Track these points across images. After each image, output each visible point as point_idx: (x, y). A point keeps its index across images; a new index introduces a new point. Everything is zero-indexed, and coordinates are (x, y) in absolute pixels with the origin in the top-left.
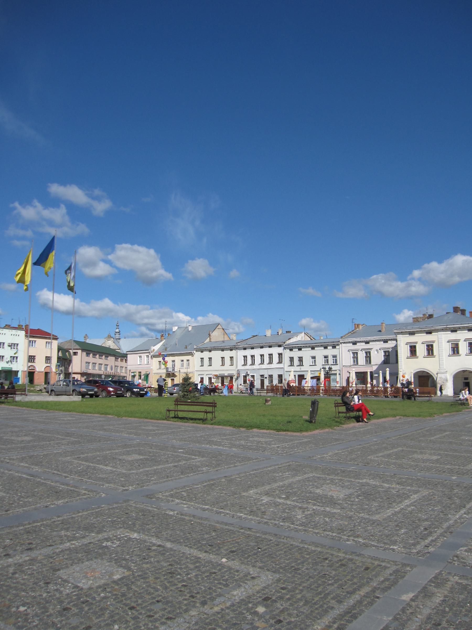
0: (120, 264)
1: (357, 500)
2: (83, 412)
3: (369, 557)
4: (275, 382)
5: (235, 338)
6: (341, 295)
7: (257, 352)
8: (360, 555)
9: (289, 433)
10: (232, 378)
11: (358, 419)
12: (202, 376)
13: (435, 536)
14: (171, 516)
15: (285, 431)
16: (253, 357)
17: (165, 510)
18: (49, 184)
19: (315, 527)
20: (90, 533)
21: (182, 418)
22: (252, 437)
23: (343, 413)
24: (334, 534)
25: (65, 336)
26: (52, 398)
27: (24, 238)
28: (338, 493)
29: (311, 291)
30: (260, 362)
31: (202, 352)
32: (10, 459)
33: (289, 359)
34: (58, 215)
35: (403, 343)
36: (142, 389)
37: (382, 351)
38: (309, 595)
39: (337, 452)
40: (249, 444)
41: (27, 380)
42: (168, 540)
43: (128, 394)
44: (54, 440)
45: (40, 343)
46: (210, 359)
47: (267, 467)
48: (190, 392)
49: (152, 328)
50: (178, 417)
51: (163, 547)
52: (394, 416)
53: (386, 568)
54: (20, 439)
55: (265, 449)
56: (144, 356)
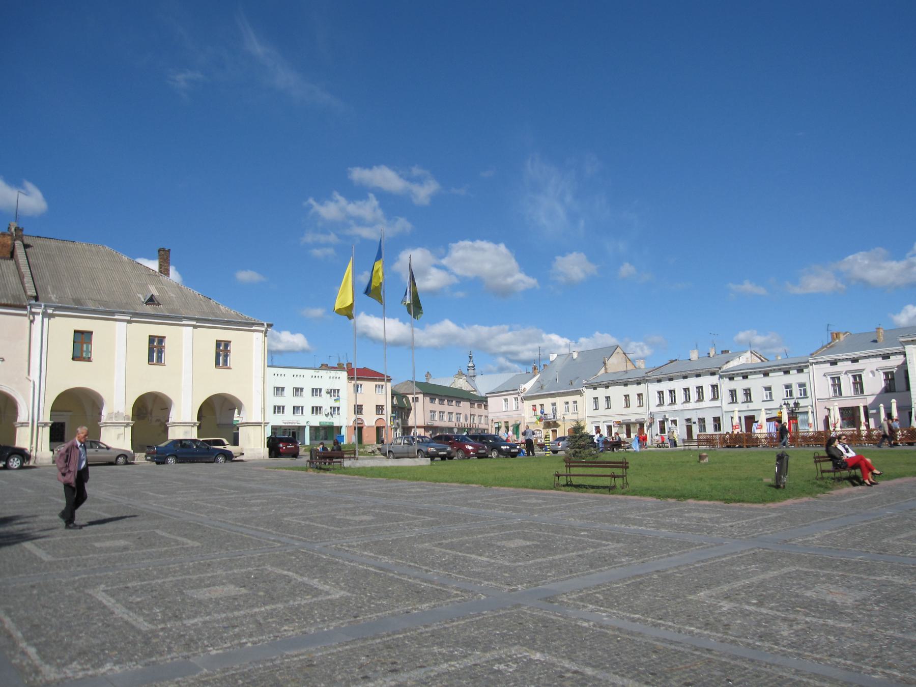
0: (458, 271)
1: (877, 608)
2: (436, 481)
4: (710, 429)
5: (643, 366)
6: (797, 290)
7: (678, 385)
9: (745, 505)
10: (642, 425)
11: (855, 481)
12: (597, 425)
15: (739, 501)
16: (672, 392)
17: (576, 620)
18: (349, 169)
19: (815, 649)
20: (473, 650)
21: (578, 486)
22: (688, 512)
23: (829, 471)
24: (849, 662)
25: (402, 374)
26: (391, 463)
27: (327, 245)
29: (748, 286)
30: (683, 399)
31: (595, 388)
32: (349, 546)
33: (729, 393)
34: (368, 209)
36: (513, 446)
37: (881, 373)
39: (828, 532)
40: (685, 522)
43: (494, 454)
44: (402, 520)
45: (368, 386)
46: (608, 398)
47: (719, 557)
48: (584, 447)
49: (516, 358)
50: (571, 485)
51: (581, 673)
54: (357, 518)
56: (511, 398)
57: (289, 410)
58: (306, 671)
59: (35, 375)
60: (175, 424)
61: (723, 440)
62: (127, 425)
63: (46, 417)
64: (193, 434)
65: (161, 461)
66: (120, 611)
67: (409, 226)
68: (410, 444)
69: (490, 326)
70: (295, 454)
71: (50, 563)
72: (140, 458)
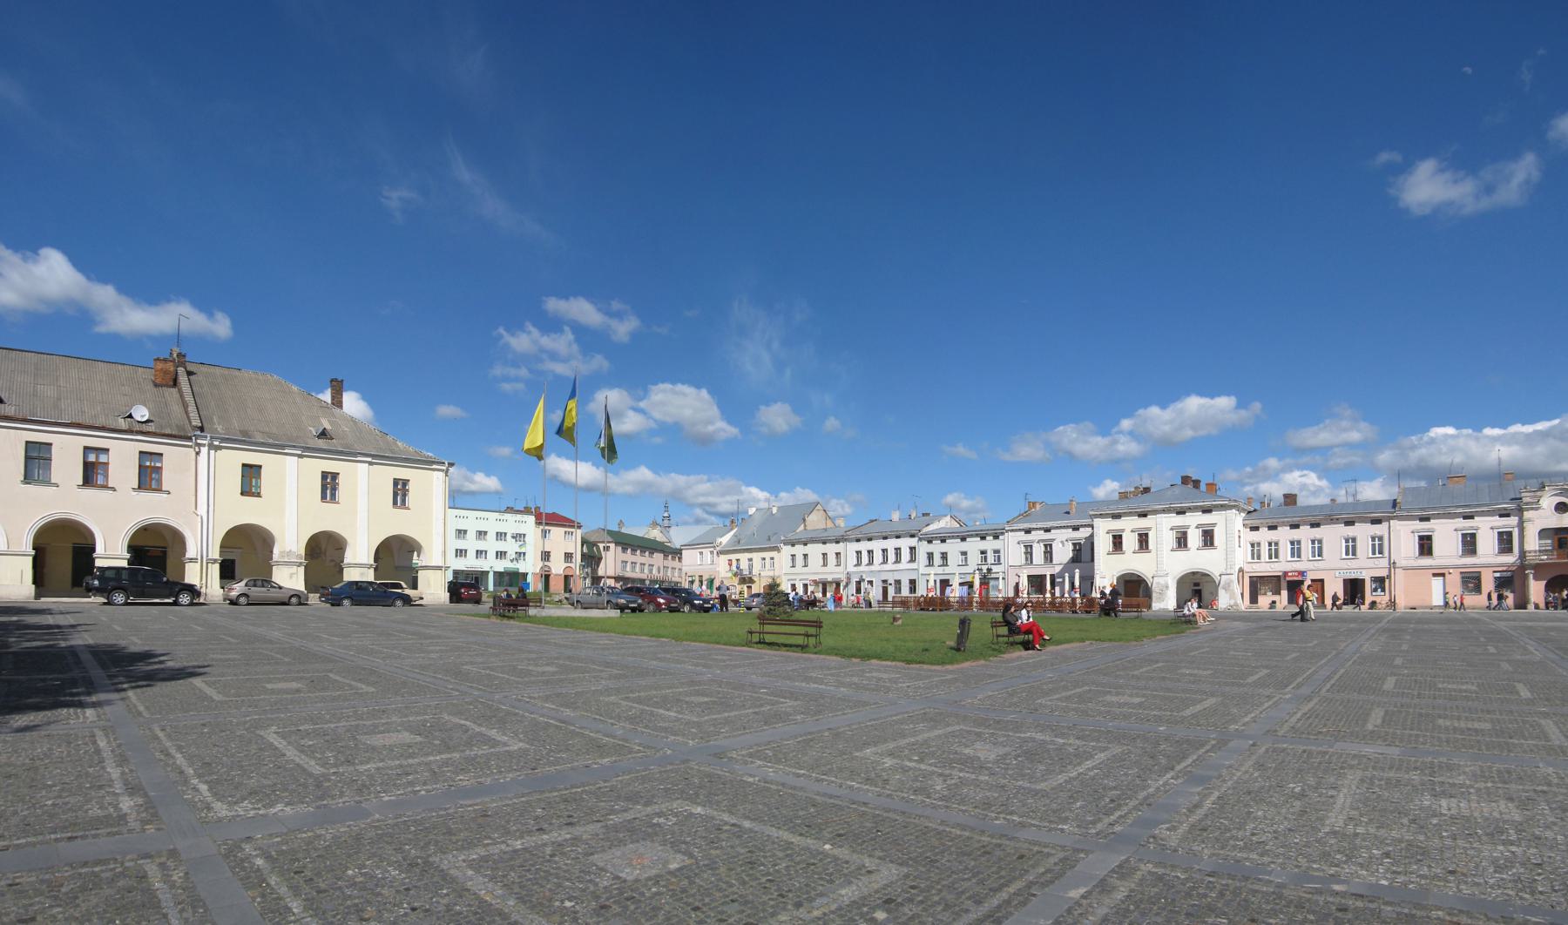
0: (657, 415)
3: (1026, 841)
4: (905, 592)
6: (1007, 457)
7: (877, 546)
8: (1012, 839)
10: (838, 585)
11: (1027, 646)
13: (1125, 809)
14: (751, 784)
19: (962, 802)
21: (770, 644)
25: (594, 520)
27: (517, 379)
28: (985, 752)
29: (961, 449)
34: (563, 342)
35: (1103, 531)
38: (950, 897)
41: (540, 587)
42: (748, 818)
43: (687, 608)
45: (557, 532)
46: (805, 556)
48: (778, 604)
52: (1083, 640)
53: (1049, 855)
54: (540, 669)
55: (888, 690)
56: (707, 552)
57: (471, 554)
58: (480, 820)
59: (202, 510)
60: (350, 566)
61: (917, 602)
62: (300, 565)
63: (215, 554)
64: (369, 576)
65: (336, 603)
66: (291, 753)
67: (606, 364)
68: (599, 594)
69: (688, 475)
70: (478, 601)
71: (221, 702)
72: (314, 598)
